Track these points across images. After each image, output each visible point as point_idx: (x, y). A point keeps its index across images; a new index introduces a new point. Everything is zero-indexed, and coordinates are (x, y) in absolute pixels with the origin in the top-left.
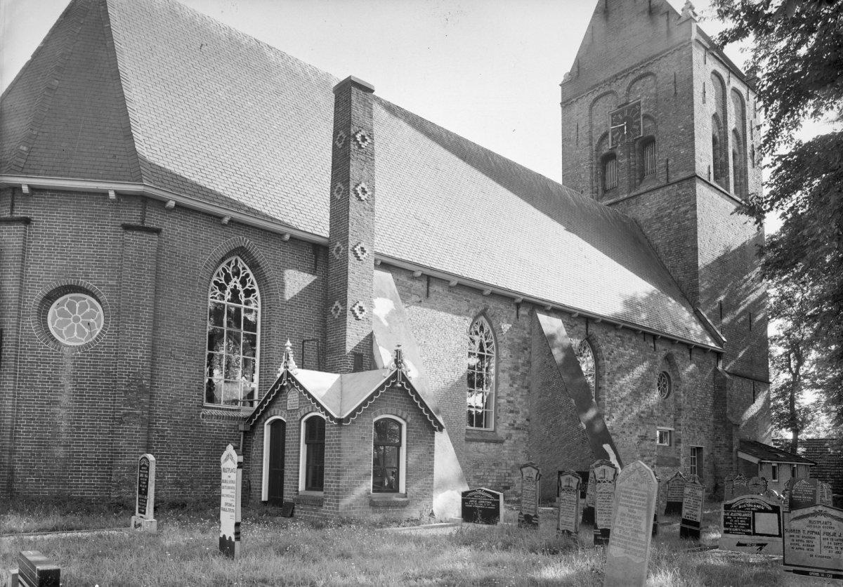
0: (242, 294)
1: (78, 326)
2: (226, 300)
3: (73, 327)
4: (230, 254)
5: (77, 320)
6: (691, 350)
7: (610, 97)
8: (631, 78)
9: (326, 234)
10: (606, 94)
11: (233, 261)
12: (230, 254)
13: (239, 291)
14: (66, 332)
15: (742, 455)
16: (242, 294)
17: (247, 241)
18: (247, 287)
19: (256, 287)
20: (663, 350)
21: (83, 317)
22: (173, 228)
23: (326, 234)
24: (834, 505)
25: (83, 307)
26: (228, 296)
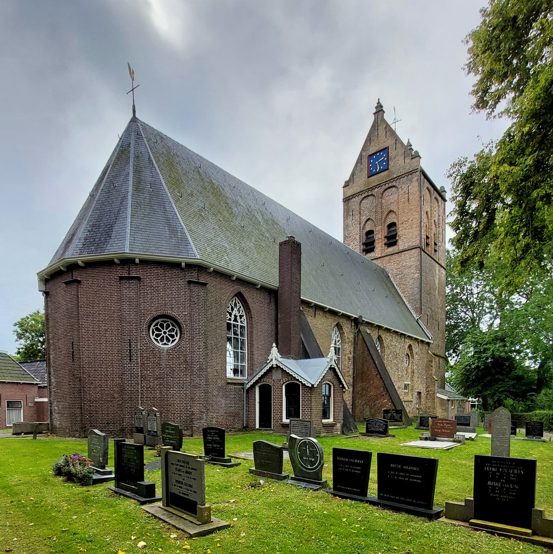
0: (238, 318)
1: (166, 336)
2: (232, 320)
3: (163, 337)
4: (234, 296)
5: (165, 333)
6: (418, 342)
7: (371, 198)
8: (384, 187)
9: (277, 284)
10: (368, 196)
11: (234, 300)
12: (234, 296)
13: (237, 316)
14: (172, 338)
15: (438, 395)
16: (238, 318)
17: (243, 290)
18: (240, 314)
19: (244, 314)
20: (408, 342)
21: (161, 331)
22: (213, 283)
23: (277, 284)
24: (205, 455)
25: (168, 326)
26: (233, 318)
